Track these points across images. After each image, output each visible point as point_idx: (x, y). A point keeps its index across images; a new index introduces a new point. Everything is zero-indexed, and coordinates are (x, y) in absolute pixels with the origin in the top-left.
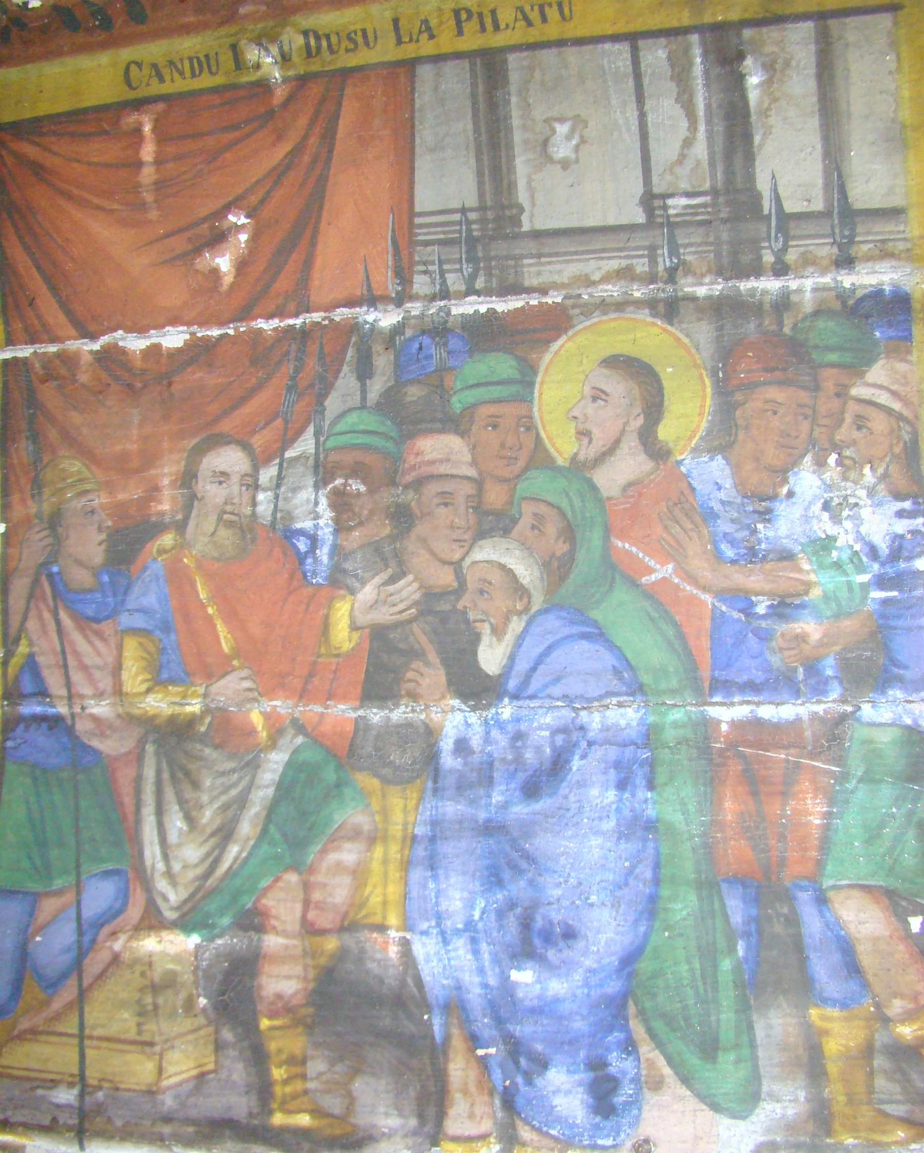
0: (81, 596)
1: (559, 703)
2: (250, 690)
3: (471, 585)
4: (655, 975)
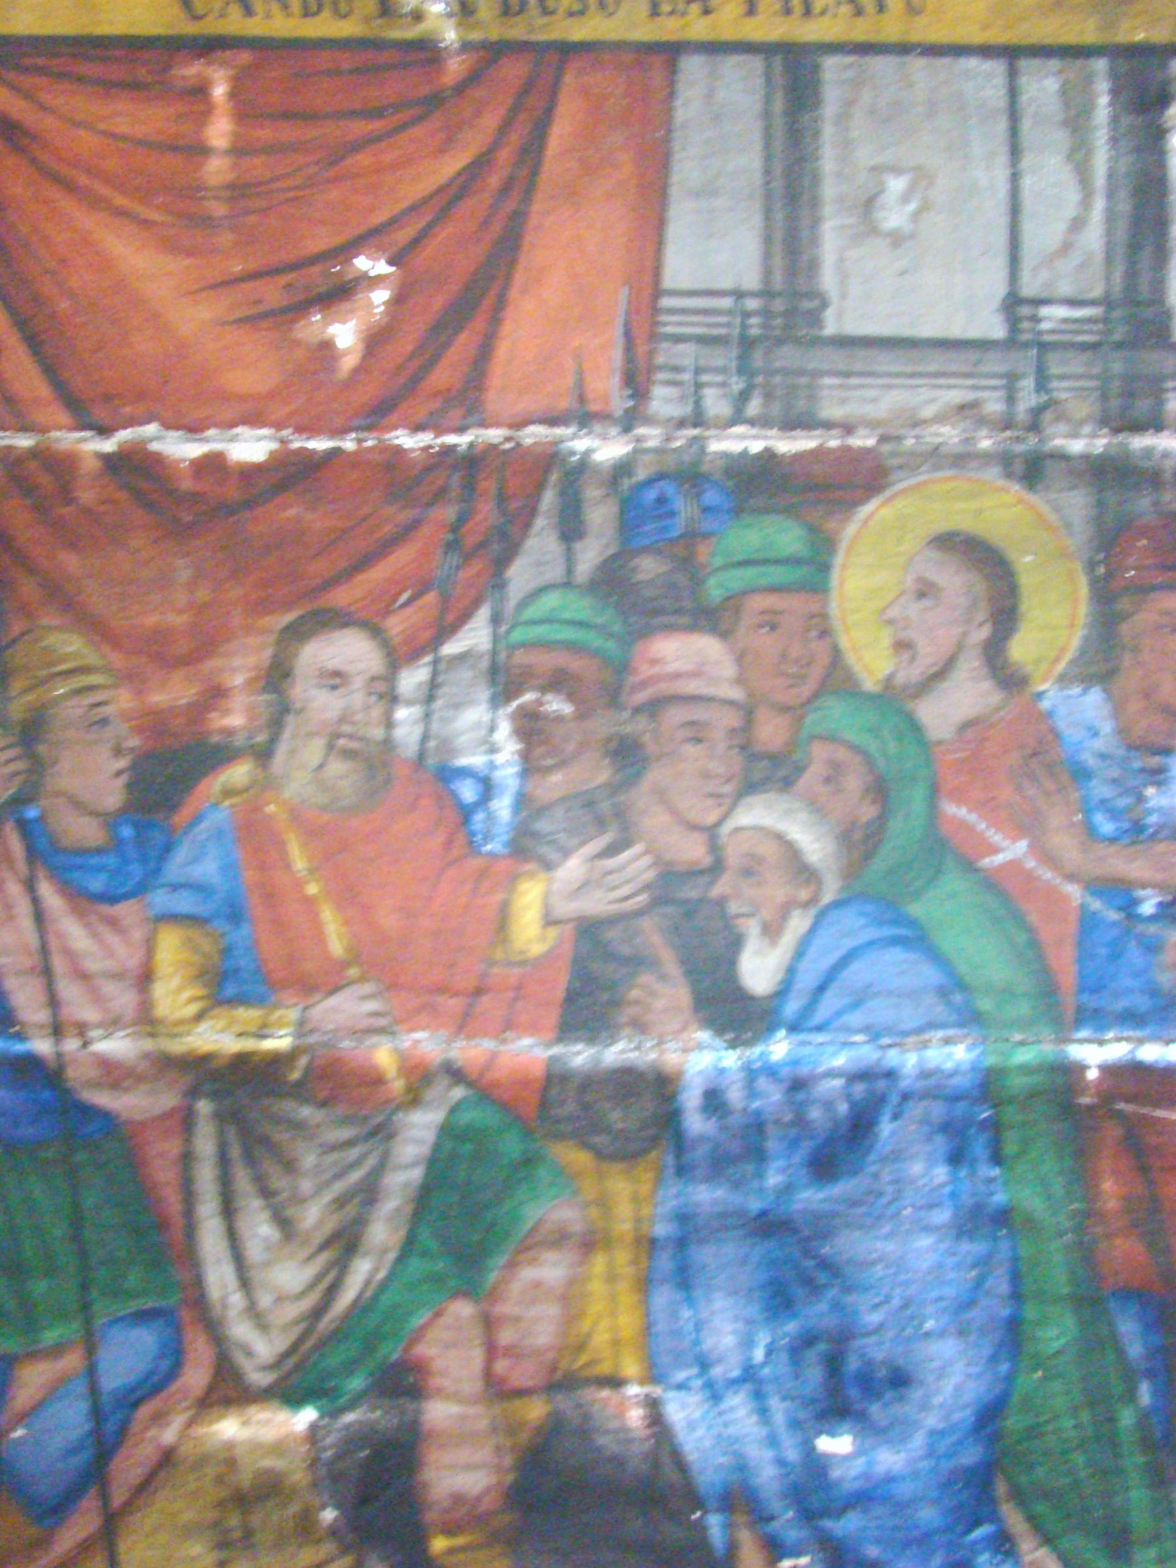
0: (79, 861)
1: (859, 1038)
2: (376, 1014)
3: (733, 858)
4: (1033, 1432)
